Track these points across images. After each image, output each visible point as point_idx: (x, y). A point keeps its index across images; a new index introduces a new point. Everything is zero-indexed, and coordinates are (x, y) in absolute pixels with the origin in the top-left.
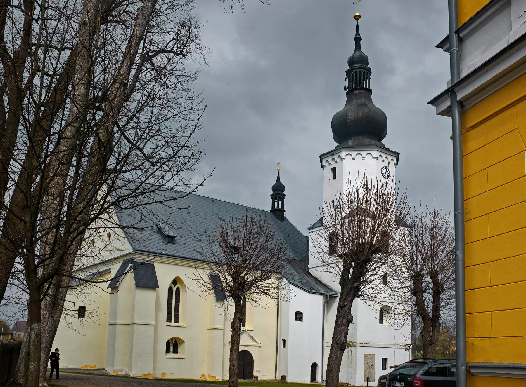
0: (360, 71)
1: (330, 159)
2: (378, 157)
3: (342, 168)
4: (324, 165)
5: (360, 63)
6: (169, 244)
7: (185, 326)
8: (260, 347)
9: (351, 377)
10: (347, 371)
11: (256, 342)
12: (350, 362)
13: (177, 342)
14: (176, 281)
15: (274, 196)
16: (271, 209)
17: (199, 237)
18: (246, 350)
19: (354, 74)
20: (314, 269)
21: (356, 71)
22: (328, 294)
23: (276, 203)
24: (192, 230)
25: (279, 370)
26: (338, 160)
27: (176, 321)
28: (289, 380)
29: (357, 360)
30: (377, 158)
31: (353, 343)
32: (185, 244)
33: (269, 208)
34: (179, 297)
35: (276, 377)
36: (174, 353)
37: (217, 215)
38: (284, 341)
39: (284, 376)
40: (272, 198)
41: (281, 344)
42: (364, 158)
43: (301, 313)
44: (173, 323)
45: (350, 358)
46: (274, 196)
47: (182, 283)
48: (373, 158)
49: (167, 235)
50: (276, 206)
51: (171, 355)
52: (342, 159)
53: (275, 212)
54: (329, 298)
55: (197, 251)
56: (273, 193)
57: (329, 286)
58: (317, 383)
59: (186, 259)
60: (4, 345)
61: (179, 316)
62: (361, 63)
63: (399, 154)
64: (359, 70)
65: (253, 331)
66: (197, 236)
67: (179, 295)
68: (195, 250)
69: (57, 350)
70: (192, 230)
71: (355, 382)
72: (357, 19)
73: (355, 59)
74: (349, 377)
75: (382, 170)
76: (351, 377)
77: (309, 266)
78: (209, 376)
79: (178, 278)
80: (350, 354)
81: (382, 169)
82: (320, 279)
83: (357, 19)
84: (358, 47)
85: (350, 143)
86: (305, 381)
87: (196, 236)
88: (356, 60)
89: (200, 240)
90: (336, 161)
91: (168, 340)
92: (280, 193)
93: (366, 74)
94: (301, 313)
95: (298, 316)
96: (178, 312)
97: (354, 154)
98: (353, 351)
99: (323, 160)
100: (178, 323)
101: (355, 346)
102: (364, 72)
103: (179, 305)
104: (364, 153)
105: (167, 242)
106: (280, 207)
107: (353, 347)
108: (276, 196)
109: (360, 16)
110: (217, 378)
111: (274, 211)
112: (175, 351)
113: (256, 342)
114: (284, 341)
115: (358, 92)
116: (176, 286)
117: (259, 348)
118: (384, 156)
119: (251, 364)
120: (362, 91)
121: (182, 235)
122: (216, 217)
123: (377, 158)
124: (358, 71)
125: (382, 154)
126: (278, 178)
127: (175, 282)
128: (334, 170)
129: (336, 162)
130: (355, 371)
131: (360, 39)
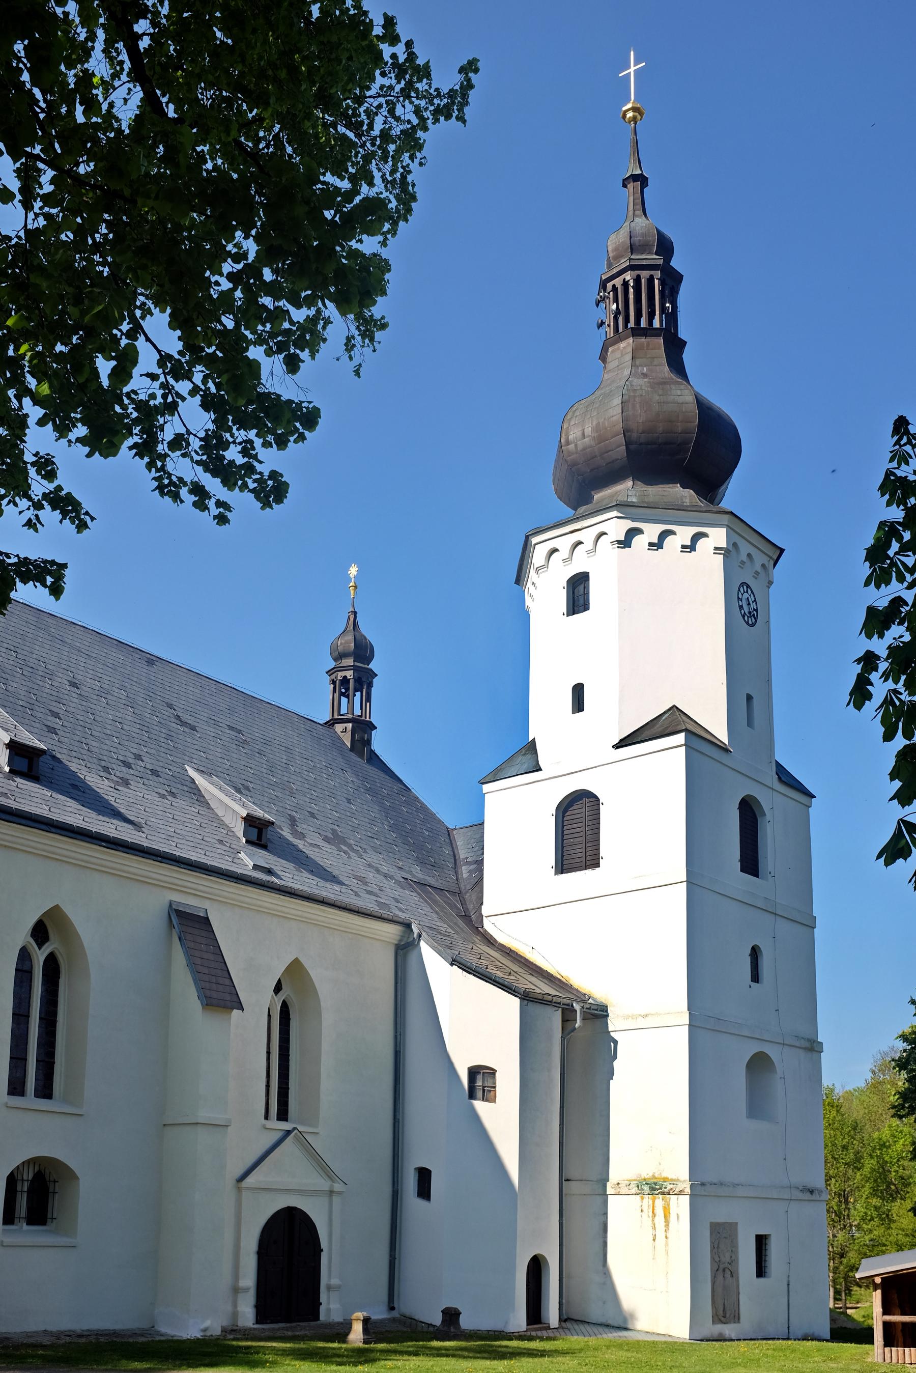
13: (47, 1176)
21: (614, 286)
41: (410, 1182)
50: (344, 710)
58: (541, 1329)
63: (782, 551)
69: (893, 437)
75: (740, 596)
79: (55, 913)
81: (739, 590)
91: (12, 1174)
114: (424, 1176)
116: (47, 949)
125: (742, 544)
127: (40, 932)
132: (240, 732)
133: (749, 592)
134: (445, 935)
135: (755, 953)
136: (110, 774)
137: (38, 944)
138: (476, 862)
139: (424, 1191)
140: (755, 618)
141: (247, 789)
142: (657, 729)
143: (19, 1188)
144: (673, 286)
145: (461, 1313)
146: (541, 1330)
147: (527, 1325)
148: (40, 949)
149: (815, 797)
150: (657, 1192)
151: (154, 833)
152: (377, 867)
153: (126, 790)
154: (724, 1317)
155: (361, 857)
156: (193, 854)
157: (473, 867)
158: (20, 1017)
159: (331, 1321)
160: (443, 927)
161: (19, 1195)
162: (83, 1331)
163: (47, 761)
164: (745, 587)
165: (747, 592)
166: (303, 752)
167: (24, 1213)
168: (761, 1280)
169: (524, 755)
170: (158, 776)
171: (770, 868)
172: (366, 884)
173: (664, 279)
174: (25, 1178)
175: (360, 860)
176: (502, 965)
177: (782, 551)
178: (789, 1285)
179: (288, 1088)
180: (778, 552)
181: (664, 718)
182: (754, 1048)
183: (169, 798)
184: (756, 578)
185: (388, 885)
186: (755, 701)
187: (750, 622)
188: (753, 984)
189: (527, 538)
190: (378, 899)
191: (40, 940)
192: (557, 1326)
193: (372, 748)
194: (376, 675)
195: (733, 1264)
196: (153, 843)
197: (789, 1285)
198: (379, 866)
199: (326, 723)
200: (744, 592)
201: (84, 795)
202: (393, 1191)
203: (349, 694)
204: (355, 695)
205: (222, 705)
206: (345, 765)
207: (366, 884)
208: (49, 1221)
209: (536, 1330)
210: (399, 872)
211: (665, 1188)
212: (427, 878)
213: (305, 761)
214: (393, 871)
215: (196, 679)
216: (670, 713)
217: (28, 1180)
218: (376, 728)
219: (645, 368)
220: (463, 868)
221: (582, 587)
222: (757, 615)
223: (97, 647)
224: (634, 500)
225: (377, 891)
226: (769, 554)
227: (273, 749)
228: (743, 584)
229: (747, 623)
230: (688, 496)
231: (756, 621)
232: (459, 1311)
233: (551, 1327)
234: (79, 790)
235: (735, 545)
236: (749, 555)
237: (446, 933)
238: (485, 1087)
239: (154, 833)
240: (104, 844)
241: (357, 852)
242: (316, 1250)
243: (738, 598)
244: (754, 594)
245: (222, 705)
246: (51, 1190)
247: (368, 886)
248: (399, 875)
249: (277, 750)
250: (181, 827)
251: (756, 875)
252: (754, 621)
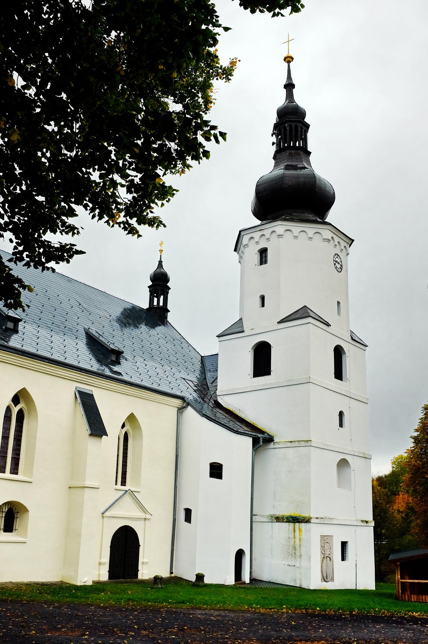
18: (128, 526)
23: (156, 299)
33: (145, 305)
38: (188, 512)
39: (202, 574)
40: (150, 291)
41: (182, 515)
48: (324, 239)
50: (155, 303)
60: (425, 594)
64: (295, 124)
72: (289, 62)
77: (218, 393)
81: (334, 257)
83: (289, 62)
84: (290, 96)
86: (226, 580)
102: (301, 128)
106: (161, 304)
108: (158, 288)
114: (188, 512)
115: (293, 152)
124: (293, 125)
128: (263, 252)
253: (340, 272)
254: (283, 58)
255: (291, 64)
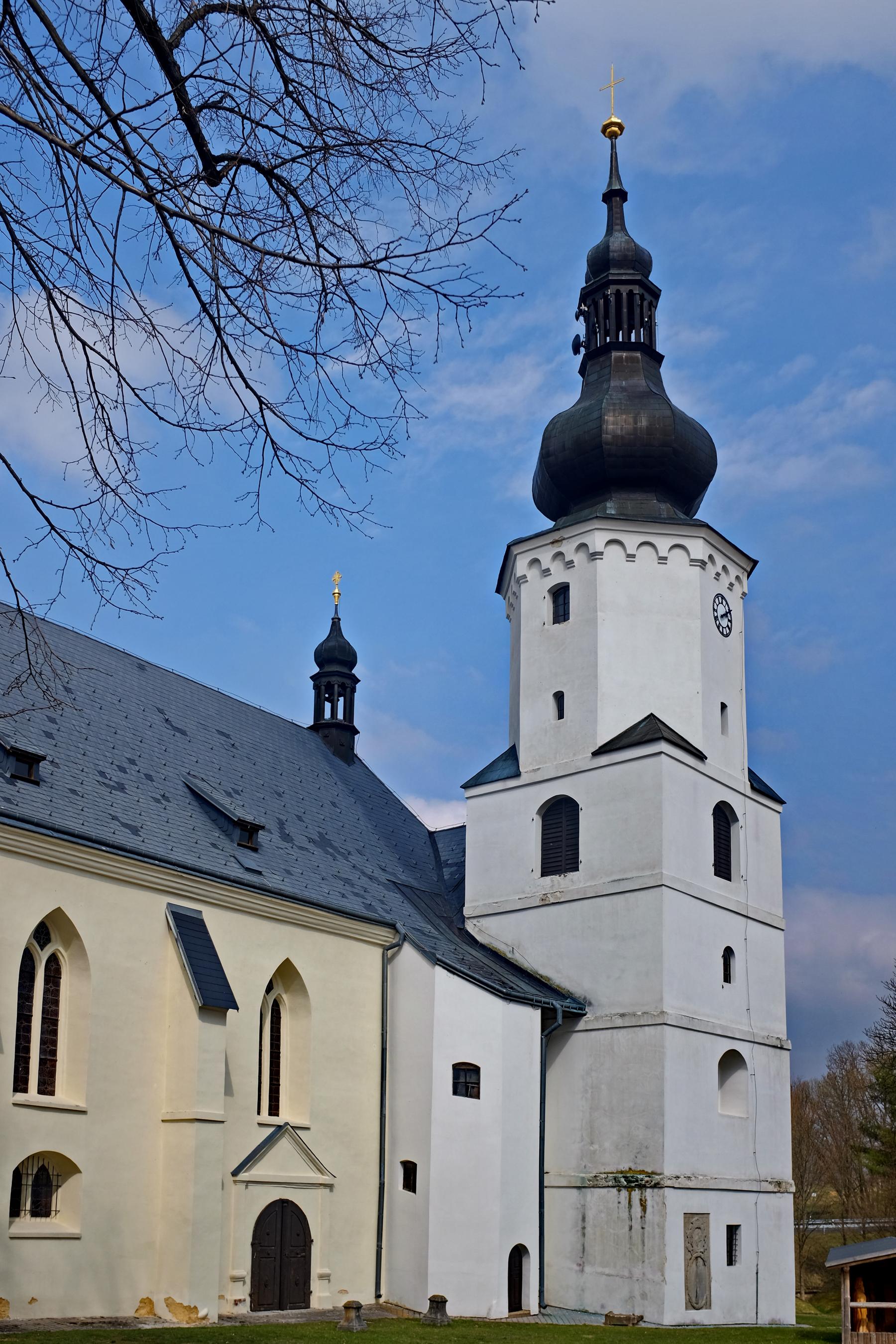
0: (631, 291)
1: (546, 556)
2: (706, 560)
3: (591, 585)
4: (525, 576)
5: (628, 268)
6: (20, 784)
7: (82, 1104)
8: (330, 1187)
9: (644, 1296)
10: (626, 1274)
11: (319, 1167)
12: (640, 1242)
14: (47, 929)
15: (324, 681)
16: (312, 723)
17: (116, 776)
19: (612, 299)
20: (484, 922)
21: (618, 291)
22: (558, 1006)
24: (90, 749)
25: (389, 1270)
26: (579, 559)
27: (47, 1086)
28: (452, 1310)
29: (667, 1237)
30: (703, 564)
31: (649, 1175)
32: (73, 792)
33: (307, 719)
34: (57, 993)
35: (378, 1296)
36: (35, 1213)
37: (161, 711)
39: (442, 1297)
40: (316, 687)
42: (663, 560)
43: (476, 1070)
44: (33, 1095)
45: (637, 1226)
46: (324, 681)
47: (71, 935)
48: (692, 560)
49: (12, 747)
50: (327, 715)
51: (27, 1224)
52: (595, 556)
53: (326, 732)
54: (564, 1017)
55: (119, 821)
56: (316, 670)
57: (549, 979)
58: (522, 1316)
59: (90, 844)
61: (54, 1066)
62: (633, 269)
63: (755, 563)
65: (84, 1112)
66: (109, 771)
67: (58, 984)
68: (114, 818)
70: (90, 749)
71: (661, 1313)
72: (613, 136)
73: (614, 251)
74: (637, 1293)
76: (644, 1296)
77: (467, 912)
78: (170, 1303)
79: (57, 915)
80: (639, 1215)
81: (714, 601)
82: (509, 955)
83: (613, 136)
84: (615, 221)
85: (611, 508)
87: (105, 770)
88: (615, 254)
89: (121, 788)
90: (572, 562)
92: (345, 670)
93: (645, 303)
94: (476, 1070)
95: (462, 1080)
96: (54, 1053)
97: (631, 541)
98: (649, 1203)
99: (518, 557)
100: (52, 1093)
101: (657, 1186)
103: (55, 1023)
104: (663, 544)
105: (12, 776)
106: (340, 716)
107: (648, 1190)
109: (621, 127)
110: (202, 1313)
111: (319, 726)
112: (42, 1209)
113: (319, 1167)
114: (410, 1170)
117: (328, 1190)
118: (720, 561)
119: (304, 1251)
120: (638, 355)
121: (57, 760)
122: (157, 719)
123: (703, 564)
125: (718, 558)
126: (336, 624)
127: (42, 934)
129: (570, 564)
130: (660, 1274)
131: (623, 195)
132: (228, 736)
133: (724, 603)
134: (429, 936)
135: (728, 953)
136: (107, 778)
137: (40, 946)
138: (456, 864)
139: (410, 1183)
140: (729, 629)
141: (237, 792)
142: (634, 738)
143: (24, 1182)
144: (651, 300)
145: (447, 1301)
146: (522, 1317)
147: (509, 1312)
148: (42, 950)
149: (786, 803)
150: (633, 1185)
151: (151, 837)
152: (363, 870)
153: (122, 794)
154: (697, 1304)
155: (346, 859)
156: (188, 857)
157: (453, 869)
158: (24, 1018)
159: (127, 1311)
160: (428, 928)
161: (24, 1188)
162: (87, 1318)
163: (46, 766)
164: (720, 598)
165: (722, 603)
166: (291, 756)
167: (28, 1207)
168: (731, 1267)
169: (505, 760)
170: (152, 780)
171: (742, 873)
172: (352, 885)
173: (643, 295)
174: (30, 1172)
175: (346, 862)
176: (484, 965)
177: (755, 563)
178: (757, 1273)
179: (279, 1085)
180: (751, 565)
181: (641, 726)
182: (729, 1045)
183: (163, 802)
184: (718, 580)
185: (373, 887)
186: (729, 710)
187: (725, 633)
188: (726, 984)
189: (509, 547)
190: (365, 901)
191: (42, 942)
192: (537, 1312)
193: (355, 752)
194: (359, 681)
195: (705, 1253)
196: (149, 847)
197: (757, 1273)
198: (364, 868)
199: (308, 728)
200: (719, 603)
201: (141, 817)
202: (380, 1184)
203: (333, 699)
204: (338, 700)
205: (211, 710)
206: (329, 769)
207: (352, 885)
208: (53, 1213)
209: (516, 1316)
210: (383, 874)
211: (641, 1180)
212: (410, 879)
213: (292, 764)
214: (378, 873)
215: (185, 684)
216: (647, 721)
217: (32, 1174)
218: (359, 732)
219: (624, 382)
220: (444, 870)
221: (562, 596)
222: (731, 626)
223: (90, 653)
224: (613, 512)
225: (362, 893)
226: (745, 567)
227: (261, 753)
228: (718, 595)
229: (722, 633)
230: (665, 508)
231: (730, 631)
232: (445, 1298)
233: (532, 1314)
234: (78, 795)
235: (711, 557)
236: (724, 568)
237: (429, 934)
238: (469, 1083)
239: (151, 837)
240: (104, 848)
241: (342, 854)
242: (307, 1241)
243: (714, 609)
244: (728, 606)
245: (211, 710)
246: (54, 1183)
247: (355, 888)
248: (383, 877)
249: (265, 754)
250: (176, 831)
251: (729, 878)
252: (728, 631)
253: (727, 636)
254: (600, 128)
255: (619, 141)
